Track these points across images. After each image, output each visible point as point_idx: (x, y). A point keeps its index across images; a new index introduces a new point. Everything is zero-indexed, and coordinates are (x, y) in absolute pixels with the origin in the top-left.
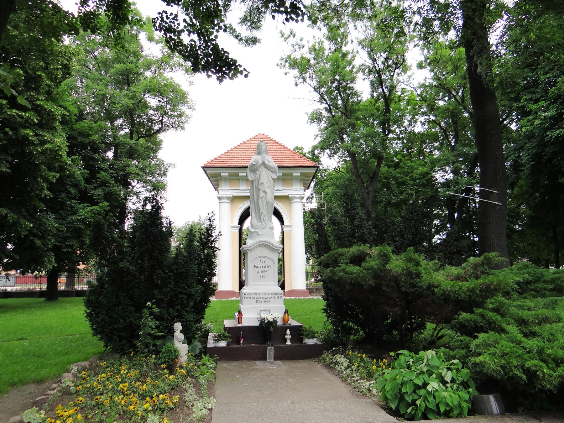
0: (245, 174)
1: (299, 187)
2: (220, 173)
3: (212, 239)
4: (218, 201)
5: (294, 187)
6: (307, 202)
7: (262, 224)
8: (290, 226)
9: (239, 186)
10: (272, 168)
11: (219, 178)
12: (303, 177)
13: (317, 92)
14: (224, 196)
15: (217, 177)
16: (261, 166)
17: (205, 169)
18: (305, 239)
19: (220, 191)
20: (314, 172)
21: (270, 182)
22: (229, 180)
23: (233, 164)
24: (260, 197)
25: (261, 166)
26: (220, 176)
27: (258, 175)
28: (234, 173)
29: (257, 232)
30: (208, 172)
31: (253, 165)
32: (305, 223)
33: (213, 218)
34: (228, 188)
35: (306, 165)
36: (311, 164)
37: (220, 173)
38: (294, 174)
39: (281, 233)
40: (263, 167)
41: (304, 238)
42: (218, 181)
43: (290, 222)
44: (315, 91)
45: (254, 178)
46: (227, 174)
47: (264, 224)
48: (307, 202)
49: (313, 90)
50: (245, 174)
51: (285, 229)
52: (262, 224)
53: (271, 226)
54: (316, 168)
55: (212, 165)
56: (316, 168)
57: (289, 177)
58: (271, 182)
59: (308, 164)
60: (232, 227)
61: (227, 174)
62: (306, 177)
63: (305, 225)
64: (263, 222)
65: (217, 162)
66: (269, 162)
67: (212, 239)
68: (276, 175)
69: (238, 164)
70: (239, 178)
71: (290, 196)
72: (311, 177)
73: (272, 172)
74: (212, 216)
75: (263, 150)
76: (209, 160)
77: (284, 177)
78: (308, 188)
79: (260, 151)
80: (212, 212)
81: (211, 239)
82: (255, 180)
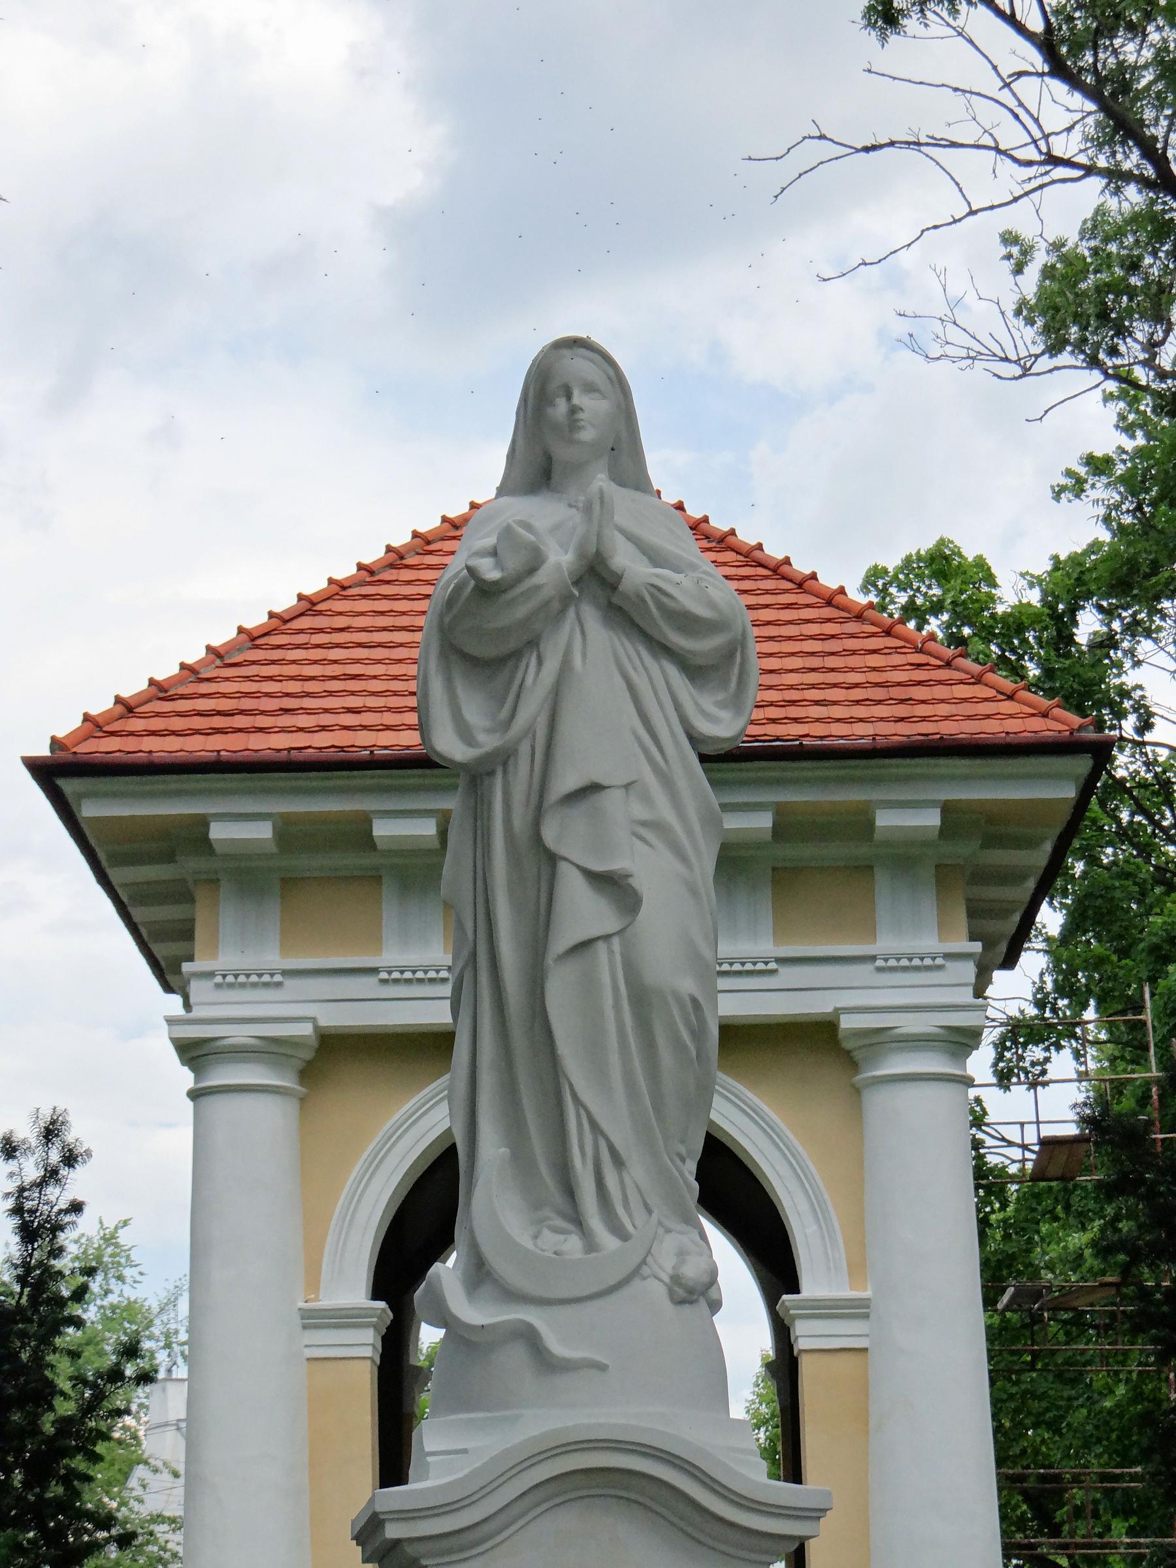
0: (427, 829)
1: (929, 942)
2: (203, 822)
3: (48, 1425)
4: (186, 1078)
5: (886, 943)
6: (1004, 1078)
7: (591, 1245)
8: (857, 1310)
9: (374, 941)
10: (688, 622)
11: (190, 865)
12: (965, 850)
13: (1072, 79)
14: (240, 1035)
15: (169, 857)
16: (567, 600)
17: (69, 786)
18: (998, 1430)
19: (197, 989)
20: (1069, 792)
21: (667, 781)
22: (290, 884)
23: (322, 740)
24: (562, 941)
25: (567, 600)
26: (203, 844)
27: (532, 708)
28: (311, 818)
29: (530, 1337)
30: (89, 810)
31: (486, 591)
32: (983, 1287)
33: (58, 1196)
34: (272, 958)
35: (992, 729)
36: (1037, 724)
37: (203, 822)
38: (885, 820)
39: (772, 1368)
40: (591, 615)
41: (988, 1425)
42: (182, 894)
43: (858, 1268)
44: (1059, 69)
45: (488, 742)
46: (263, 831)
47: (609, 1242)
48: (1004, 1078)
49: (1036, 59)
50: (427, 829)
51: (806, 1335)
52: (591, 1245)
53: (692, 1271)
54: (1083, 765)
55: (130, 744)
56: (1083, 765)
57: (836, 851)
58: (682, 783)
59: (1013, 725)
60: (314, 1319)
61: (263, 831)
62: (993, 841)
63: (989, 1301)
64: (595, 1222)
65: (178, 724)
66: (655, 557)
67: (48, 1425)
68: (735, 703)
69: (364, 738)
70: (367, 860)
71: (847, 1023)
72: (1031, 843)
73: (695, 671)
74: (51, 1175)
75: (587, 435)
76: (101, 705)
77: (790, 852)
78: (1010, 961)
79: (562, 452)
80: (50, 1133)
81: (34, 1430)
82: (503, 758)
